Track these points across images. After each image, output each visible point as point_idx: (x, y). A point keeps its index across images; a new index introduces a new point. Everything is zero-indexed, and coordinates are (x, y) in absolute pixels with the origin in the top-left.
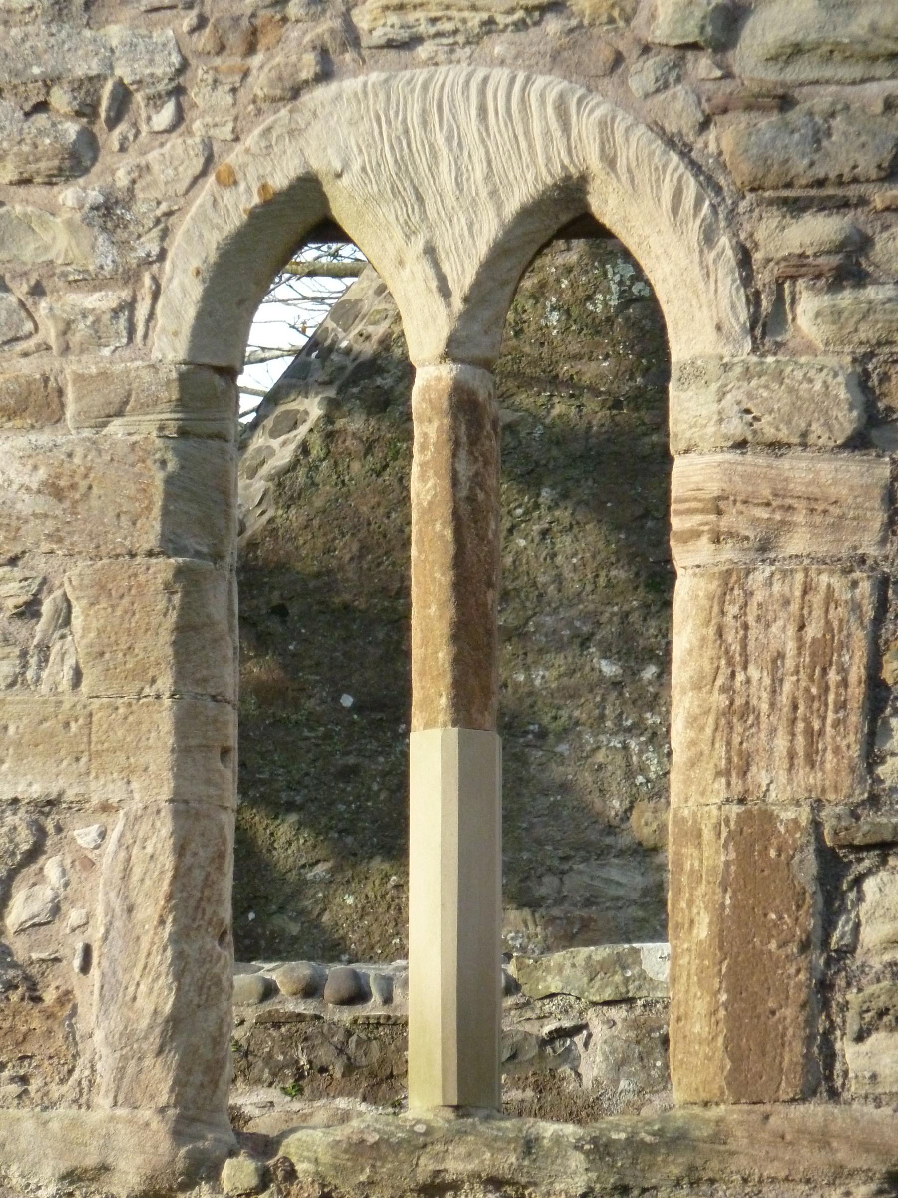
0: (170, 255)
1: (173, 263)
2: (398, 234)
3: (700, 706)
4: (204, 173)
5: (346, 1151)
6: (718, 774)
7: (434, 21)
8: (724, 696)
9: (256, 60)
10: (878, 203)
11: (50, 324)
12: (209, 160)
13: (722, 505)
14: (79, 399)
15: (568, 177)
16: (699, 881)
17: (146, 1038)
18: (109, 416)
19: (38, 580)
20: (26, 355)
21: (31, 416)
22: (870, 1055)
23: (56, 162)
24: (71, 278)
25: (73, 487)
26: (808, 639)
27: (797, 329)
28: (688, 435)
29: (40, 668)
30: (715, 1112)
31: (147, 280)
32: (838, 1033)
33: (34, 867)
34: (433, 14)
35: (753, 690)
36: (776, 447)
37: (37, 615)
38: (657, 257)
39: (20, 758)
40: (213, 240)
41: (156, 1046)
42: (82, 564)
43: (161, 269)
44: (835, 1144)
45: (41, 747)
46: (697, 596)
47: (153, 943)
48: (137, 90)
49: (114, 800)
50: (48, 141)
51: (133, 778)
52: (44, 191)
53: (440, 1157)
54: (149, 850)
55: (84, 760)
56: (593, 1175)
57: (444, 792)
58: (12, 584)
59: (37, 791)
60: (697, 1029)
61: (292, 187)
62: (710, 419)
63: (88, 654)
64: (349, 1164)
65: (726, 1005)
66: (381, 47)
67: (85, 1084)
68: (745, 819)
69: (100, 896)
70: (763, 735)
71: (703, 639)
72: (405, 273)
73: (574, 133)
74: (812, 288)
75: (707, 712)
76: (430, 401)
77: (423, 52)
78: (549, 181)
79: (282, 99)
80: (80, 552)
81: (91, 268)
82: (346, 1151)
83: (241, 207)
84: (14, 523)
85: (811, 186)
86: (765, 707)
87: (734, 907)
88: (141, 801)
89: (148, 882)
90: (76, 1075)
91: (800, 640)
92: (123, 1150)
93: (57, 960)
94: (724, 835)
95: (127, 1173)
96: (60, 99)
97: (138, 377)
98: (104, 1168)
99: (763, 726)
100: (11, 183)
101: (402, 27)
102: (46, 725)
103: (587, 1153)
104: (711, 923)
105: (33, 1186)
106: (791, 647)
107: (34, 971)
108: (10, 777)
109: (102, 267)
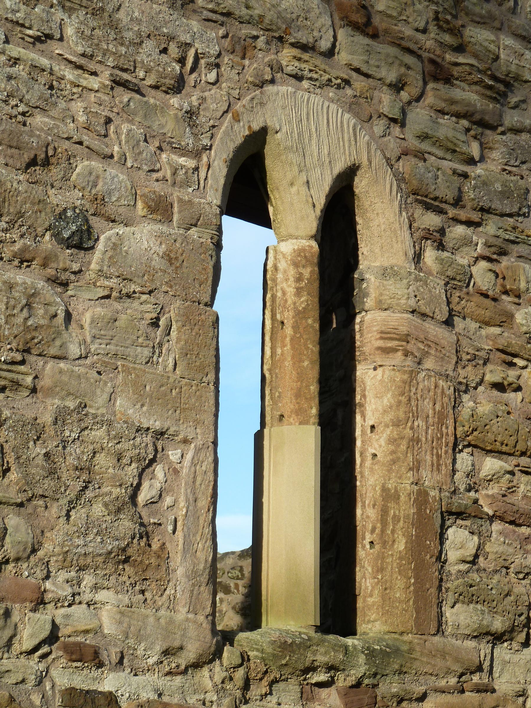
0: (213, 147)
1: (215, 152)
2: (296, 169)
3: (398, 434)
4: (226, 112)
5: (279, 647)
6: (410, 469)
7: (311, 71)
8: (411, 431)
9: (247, 62)
10: (450, 215)
11: (167, 167)
12: (229, 106)
13: (409, 338)
14: (180, 212)
15: (354, 165)
16: (399, 521)
17: (202, 575)
18: (191, 225)
19: (160, 307)
20: (157, 180)
21: (161, 214)
22: (457, 614)
23: (172, 82)
24: (174, 146)
25: (176, 258)
26: (437, 410)
27: (425, 263)
28: (389, 301)
29: (159, 356)
30: (408, 638)
31: (205, 159)
32: (444, 602)
33: (151, 469)
34: (311, 68)
35: (420, 431)
36: (424, 315)
37: (158, 326)
38: (377, 214)
39: (152, 405)
40: (232, 146)
41: (206, 580)
42: (179, 303)
43: (210, 154)
44: (447, 658)
45: (160, 400)
46: (394, 380)
47: (205, 521)
48: (202, 58)
49: (190, 437)
50: (169, 69)
51: (198, 427)
52: (163, 95)
53: (315, 653)
54: (204, 468)
55: (178, 412)
56: (367, 667)
57: (315, 459)
58: (149, 306)
59: (158, 425)
60: (398, 595)
61: (259, 130)
62: (403, 296)
63: (181, 353)
64: (280, 654)
65: (414, 584)
66: (290, 76)
67: (172, 598)
68: (419, 492)
69: (182, 490)
70: (423, 453)
71: (400, 402)
72: (294, 189)
73: (358, 144)
74: (432, 245)
75: (402, 438)
76: (305, 257)
77: (305, 84)
78: (349, 164)
79: (258, 86)
80: (179, 296)
81: (183, 143)
82: (279, 647)
83: (242, 134)
84: (152, 272)
85: (432, 199)
86: (424, 439)
87: (416, 536)
88: (201, 440)
89: (203, 486)
90: (167, 592)
91: (434, 410)
92: (190, 638)
93: (160, 524)
94: (412, 500)
95: (190, 652)
96: (174, 50)
97: (204, 208)
98: (181, 648)
99: (423, 449)
100: (150, 86)
101: (299, 69)
102: (163, 389)
103: (366, 655)
104: (406, 543)
105: (146, 656)
106: (431, 412)
107: (150, 529)
108: (147, 415)
109: (188, 144)
